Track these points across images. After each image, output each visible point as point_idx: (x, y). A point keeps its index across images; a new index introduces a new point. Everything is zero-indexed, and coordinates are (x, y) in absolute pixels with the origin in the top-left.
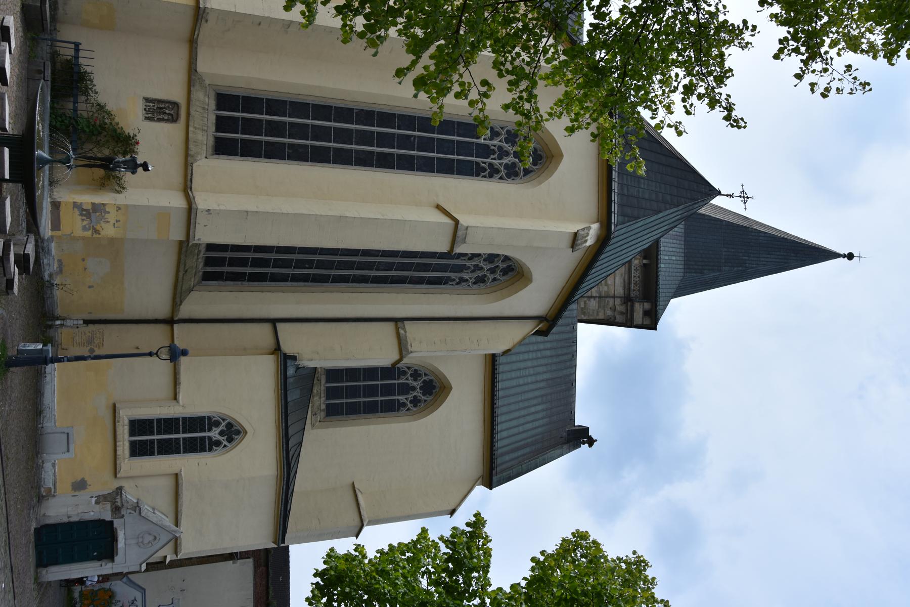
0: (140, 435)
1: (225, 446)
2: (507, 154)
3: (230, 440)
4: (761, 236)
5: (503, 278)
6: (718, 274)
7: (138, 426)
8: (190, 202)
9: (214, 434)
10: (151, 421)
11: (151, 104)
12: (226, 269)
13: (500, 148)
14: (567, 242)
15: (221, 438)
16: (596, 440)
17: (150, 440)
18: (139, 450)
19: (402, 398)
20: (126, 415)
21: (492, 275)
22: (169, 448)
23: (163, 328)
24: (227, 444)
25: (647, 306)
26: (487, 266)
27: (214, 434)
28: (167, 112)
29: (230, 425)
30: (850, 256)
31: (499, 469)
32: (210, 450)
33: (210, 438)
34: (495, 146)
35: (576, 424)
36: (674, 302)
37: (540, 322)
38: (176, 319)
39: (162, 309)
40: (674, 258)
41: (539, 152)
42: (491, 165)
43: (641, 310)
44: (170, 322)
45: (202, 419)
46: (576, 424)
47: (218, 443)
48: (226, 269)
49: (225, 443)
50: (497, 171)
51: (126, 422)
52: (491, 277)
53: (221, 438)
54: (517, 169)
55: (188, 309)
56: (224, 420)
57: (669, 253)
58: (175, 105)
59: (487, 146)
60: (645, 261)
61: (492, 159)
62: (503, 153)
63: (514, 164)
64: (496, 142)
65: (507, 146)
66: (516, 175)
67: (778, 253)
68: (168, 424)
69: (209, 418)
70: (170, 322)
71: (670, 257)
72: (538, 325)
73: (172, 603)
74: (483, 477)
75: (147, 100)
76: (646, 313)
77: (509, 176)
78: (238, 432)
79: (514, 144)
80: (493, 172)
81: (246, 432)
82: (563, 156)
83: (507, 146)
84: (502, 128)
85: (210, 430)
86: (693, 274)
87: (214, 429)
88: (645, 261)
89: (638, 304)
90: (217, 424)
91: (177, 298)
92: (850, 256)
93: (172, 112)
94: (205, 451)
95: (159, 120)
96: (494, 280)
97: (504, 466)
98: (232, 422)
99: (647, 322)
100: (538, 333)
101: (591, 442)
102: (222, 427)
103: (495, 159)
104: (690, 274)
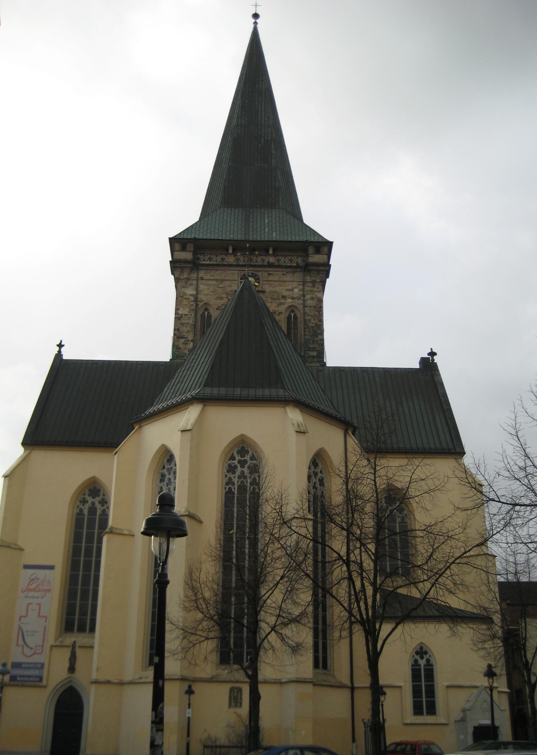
0: (423, 709)
1: (430, 656)
2: (243, 472)
3: (426, 653)
4: (241, 122)
5: (320, 465)
6: (278, 170)
7: (418, 710)
8: (290, 682)
9: (422, 662)
10: (414, 702)
11: (232, 704)
12: (321, 655)
13: (239, 477)
14: (302, 437)
15: (425, 659)
16: (432, 354)
17: (422, 696)
18: (432, 710)
19: (399, 520)
20: (411, 718)
21: (318, 475)
22: (431, 691)
23: (356, 693)
24: (428, 654)
25: (311, 250)
26: (313, 479)
27: (422, 662)
28: (236, 694)
29: (417, 653)
30: (256, 16)
31: (451, 446)
32: (432, 665)
33: (425, 666)
34: (238, 481)
35: (418, 367)
36: (307, 219)
37: (348, 433)
38: (350, 685)
39: (346, 694)
40: (267, 221)
41: (240, 449)
42: (251, 484)
43: (315, 256)
44: (353, 689)
45: (413, 670)
46: (418, 367)
47: (428, 661)
48: (321, 655)
49: (428, 656)
50: (255, 479)
51: (415, 717)
52: (320, 475)
53: (425, 659)
54: (252, 465)
55: (346, 681)
56: (414, 656)
57: (263, 228)
58: (232, 690)
59: (239, 487)
60: (271, 252)
61: (247, 483)
62: (242, 476)
63: (249, 468)
64: (235, 480)
65: (238, 473)
66: (256, 466)
67: (257, 103)
68: (416, 692)
69: (413, 666)
70: (353, 689)
71: (266, 225)
72: (350, 435)
73: (501, 710)
74: (456, 459)
75: (230, 706)
76: (318, 251)
77: (257, 472)
78: (421, 648)
79: (236, 467)
80: (256, 483)
81: (421, 643)
82: (243, 434)
83: (238, 473)
84: (226, 476)
85: (420, 665)
86: (280, 199)
87: (419, 663)
88: (271, 252)
89: (309, 258)
90: (416, 661)
91: (342, 686)
92: (256, 16)
93: (236, 692)
94: (433, 669)
95: (241, 699)
96: (321, 472)
97: (449, 441)
98: (415, 651)
99: (326, 250)
100: (353, 433)
101: (432, 354)
102: (418, 657)
103: (247, 481)
104: (281, 202)
